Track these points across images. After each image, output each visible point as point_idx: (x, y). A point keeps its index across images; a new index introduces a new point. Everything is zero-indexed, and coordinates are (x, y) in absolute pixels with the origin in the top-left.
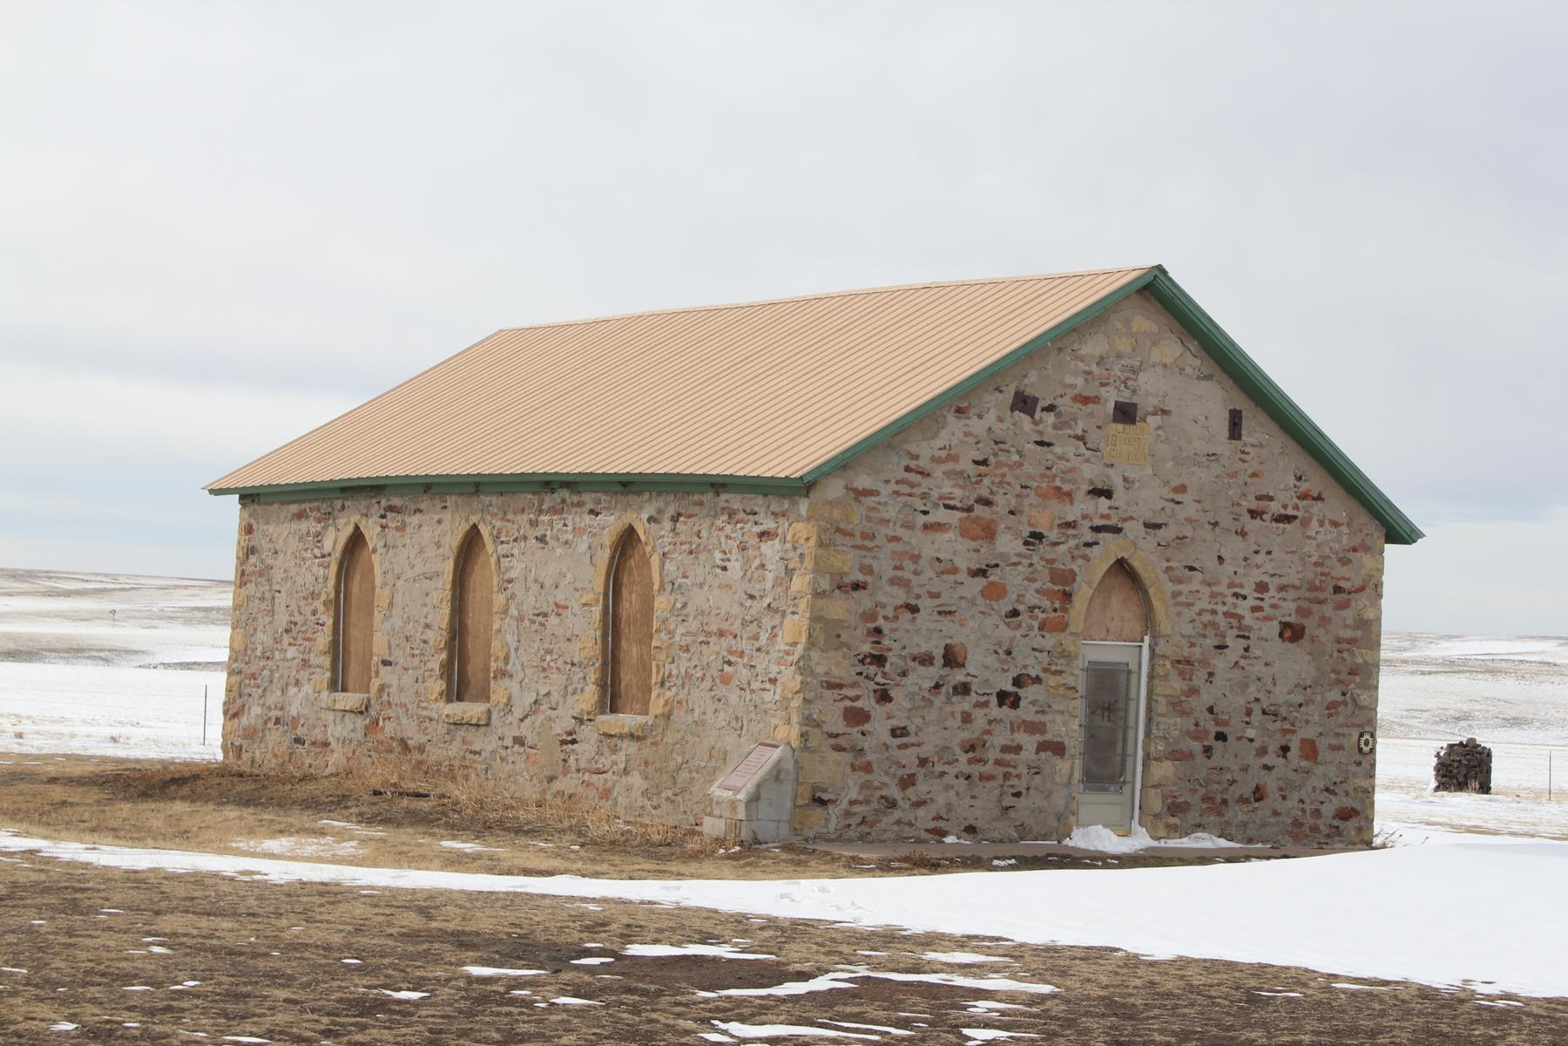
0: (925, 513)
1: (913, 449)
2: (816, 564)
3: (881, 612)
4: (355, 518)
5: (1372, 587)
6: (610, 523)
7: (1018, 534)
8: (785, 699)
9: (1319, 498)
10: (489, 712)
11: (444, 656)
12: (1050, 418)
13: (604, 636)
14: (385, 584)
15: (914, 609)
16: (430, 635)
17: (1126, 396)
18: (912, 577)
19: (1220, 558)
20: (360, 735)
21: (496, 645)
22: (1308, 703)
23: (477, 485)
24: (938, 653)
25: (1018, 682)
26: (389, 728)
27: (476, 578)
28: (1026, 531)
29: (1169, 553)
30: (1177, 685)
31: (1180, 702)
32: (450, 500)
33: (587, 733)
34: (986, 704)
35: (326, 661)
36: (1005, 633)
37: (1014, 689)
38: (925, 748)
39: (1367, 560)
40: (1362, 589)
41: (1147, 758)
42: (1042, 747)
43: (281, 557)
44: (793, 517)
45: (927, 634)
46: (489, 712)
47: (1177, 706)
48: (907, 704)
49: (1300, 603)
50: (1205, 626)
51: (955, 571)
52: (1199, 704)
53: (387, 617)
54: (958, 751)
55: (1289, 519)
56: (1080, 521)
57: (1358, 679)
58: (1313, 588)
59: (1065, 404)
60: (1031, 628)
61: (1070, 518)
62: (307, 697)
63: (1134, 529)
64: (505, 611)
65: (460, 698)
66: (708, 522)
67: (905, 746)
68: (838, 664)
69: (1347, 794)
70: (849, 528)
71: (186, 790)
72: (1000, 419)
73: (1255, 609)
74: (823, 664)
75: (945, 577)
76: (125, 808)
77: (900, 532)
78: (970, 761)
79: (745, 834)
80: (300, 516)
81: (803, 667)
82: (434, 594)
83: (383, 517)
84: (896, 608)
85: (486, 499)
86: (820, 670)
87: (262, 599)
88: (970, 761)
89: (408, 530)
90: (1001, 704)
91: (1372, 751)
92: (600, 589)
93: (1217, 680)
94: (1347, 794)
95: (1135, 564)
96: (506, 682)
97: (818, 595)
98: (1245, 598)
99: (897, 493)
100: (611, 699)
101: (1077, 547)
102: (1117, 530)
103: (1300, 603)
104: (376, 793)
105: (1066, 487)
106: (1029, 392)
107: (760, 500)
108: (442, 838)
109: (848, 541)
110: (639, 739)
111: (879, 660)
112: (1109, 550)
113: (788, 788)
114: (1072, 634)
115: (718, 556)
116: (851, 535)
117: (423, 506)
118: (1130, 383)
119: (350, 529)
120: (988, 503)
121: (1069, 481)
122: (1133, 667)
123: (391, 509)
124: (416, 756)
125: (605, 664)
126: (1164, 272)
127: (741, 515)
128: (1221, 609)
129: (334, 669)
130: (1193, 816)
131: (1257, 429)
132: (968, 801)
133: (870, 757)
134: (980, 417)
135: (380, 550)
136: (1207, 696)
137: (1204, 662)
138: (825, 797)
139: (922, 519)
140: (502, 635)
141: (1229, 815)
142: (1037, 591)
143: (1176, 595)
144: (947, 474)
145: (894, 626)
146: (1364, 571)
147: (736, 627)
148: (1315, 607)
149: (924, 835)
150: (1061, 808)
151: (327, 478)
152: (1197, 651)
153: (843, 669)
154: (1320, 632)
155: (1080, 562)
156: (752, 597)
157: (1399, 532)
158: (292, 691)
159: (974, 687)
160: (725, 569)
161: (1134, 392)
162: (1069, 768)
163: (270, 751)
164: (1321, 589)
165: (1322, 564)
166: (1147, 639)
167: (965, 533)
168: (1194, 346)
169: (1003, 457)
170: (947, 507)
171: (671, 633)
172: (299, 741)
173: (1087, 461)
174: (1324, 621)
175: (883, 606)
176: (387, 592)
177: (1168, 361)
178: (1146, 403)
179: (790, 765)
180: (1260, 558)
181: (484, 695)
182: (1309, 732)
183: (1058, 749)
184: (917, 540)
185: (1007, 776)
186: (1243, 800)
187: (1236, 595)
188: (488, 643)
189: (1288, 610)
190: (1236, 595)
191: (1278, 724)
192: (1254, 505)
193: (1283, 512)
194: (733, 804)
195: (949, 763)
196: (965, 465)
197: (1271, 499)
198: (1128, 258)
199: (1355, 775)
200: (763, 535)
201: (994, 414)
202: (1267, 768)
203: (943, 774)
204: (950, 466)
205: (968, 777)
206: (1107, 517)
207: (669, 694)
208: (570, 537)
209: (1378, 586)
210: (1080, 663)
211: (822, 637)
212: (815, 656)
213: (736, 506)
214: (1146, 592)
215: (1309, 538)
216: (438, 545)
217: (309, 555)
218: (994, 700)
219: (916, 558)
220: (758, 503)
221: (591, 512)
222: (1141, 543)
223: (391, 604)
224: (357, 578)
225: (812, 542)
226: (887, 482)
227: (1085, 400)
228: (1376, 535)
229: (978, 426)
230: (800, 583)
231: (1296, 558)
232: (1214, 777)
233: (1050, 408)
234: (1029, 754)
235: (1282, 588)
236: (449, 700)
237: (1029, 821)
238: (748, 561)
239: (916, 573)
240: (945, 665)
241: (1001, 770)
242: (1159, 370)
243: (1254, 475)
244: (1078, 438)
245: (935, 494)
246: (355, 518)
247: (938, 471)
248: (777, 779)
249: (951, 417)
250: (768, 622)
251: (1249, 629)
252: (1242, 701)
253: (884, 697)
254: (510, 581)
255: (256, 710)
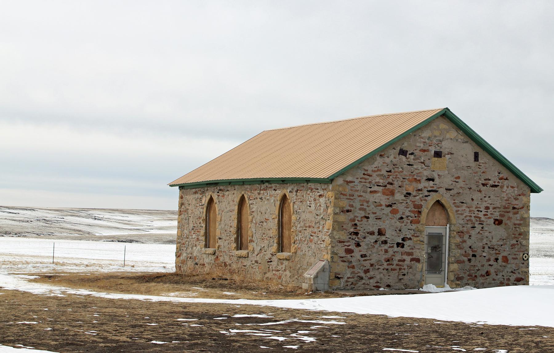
0: (370, 188)
1: (366, 168)
2: (334, 204)
3: (357, 219)
4: (211, 193)
5: (527, 207)
6: (279, 193)
7: (402, 193)
8: (326, 246)
9: (507, 179)
10: (248, 253)
11: (235, 236)
12: (412, 157)
13: (279, 228)
14: (219, 214)
15: (368, 218)
16: (232, 229)
17: (438, 149)
18: (367, 208)
19: (472, 199)
20: (213, 262)
21: (249, 232)
22: (505, 244)
23: (243, 182)
24: (376, 232)
25: (403, 239)
26: (221, 259)
27: (244, 212)
28: (405, 192)
29: (454, 198)
30: (458, 240)
31: (460, 245)
32: (236, 187)
33: (275, 259)
34: (393, 247)
35: (203, 238)
36: (398, 224)
37: (402, 242)
38: (372, 261)
39: (524, 199)
40: (523, 208)
41: (449, 263)
42: (412, 260)
43: (191, 206)
44: (328, 190)
45: (372, 225)
46: (248, 253)
47: (458, 246)
48: (366, 247)
49: (501, 213)
50: (468, 221)
51: (381, 205)
52: (466, 246)
53: (220, 224)
54: (383, 261)
55: (496, 186)
56: (423, 189)
57: (522, 237)
58: (505, 208)
59: (417, 153)
60: (407, 223)
61: (420, 188)
62: (198, 250)
63: (442, 191)
64: (252, 221)
65: (241, 249)
66: (305, 192)
67: (366, 260)
68: (343, 235)
69: (519, 273)
70: (345, 193)
71: (159, 280)
72: (395, 158)
73: (485, 215)
74: (338, 235)
75: (378, 207)
76: (136, 285)
77: (362, 194)
78: (388, 265)
79: (313, 288)
80: (196, 193)
81: (331, 236)
82: (232, 216)
83: (218, 192)
84: (361, 218)
85: (246, 186)
86: (337, 237)
87: (186, 219)
88: (388, 265)
89: (225, 196)
90: (398, 247)
91: (528, 259)
92: (277, 214)
93: (472, 238)
94: (519, 273)
95: (443, 202)
96: (252, 244)
97: (335, 214)
98: (481, 211)
99: (361, 182)
100: (281, 248)
101: (423, 197)
102: (436, 191)
103: (501, 213)
104: (214, 279)
105: (418, 178)
106: (404, 149)
107: (319, 185)
108: (225, 291)
109: (345, 197)
110: (288, 260)
111: (356, 234)
112: (434, 197)
113: (327, 274)
114: (422, 224)
115: (308, 202)
116: (346, 195)
117: (229, 189)
118: (439, 145)
119: (209, 196)
120: (391, 184)
121: (419, 176)
122: (444, 234)
123: (220, 190)
124: (228, 267)
125: (279, 237)
126: (449, 110)
127: (314, 190)
128: (473, 215)
129: (206, 241)
130: (465, 281)
131: (484, 158)
132: (387, 277)
133: (354, 264)
134: (388, 157)
135: (218, 203)
136: (469, 243)
137: (468, 232)
138: (339, 276)
139: (369, 190)
140: (251, 229)
141: (477, 280)
142: (409, 211)
143: (457, 211)
144: (378, 175)
145: (361, 223)
146: (523, 202)
147: (313, 225)
148: (506, 214)
149: (373, 288)
150: (419, 279)
151: (253, 177)
152: (465, 229)
153: (344, 236)
154: (508, 222)
155: (424, 202)
156: (317, 215)
157: (535, 189)
158: (194, 248)
159: (388, 242)
160: (310, 206)
161: (441, 148)
162: (423, 266)
163: (188, 267)
164: (508, 208)
165: (508, 200)
166: (448, 225)
167: (384, 193)
168: (461, 132)
169: (396, 170)
170: (378, 185)
171: (296, 227)
172: (197, 264)
173: (425, 170)
174: (509, 218)
175: (357, 217)
176: (220, 216)
177: (452, 138)
178: (444, 151)
179: (327, 267)
180: (486, 199)
181: (247, 248)
182: (505, 254)
183: (418, 260)
184: (368, 196)
185: (400, 269)
186: (482, 276)
187: (478, 211)
188: (248, 231)
189: (497, 215)
190: (478, 211)
191: (494, 252)
192: (484, 182)
193: (494, 184)
194: (310, 278)
195: (380, 265)
196: (384, 172)
197: (490, 180)
198: (438, 106)
199: (522, 267)
200: (320, 196)
201: (393, 156)
202: (490, 265)
203: (379, 269)
204: (379, 173)
205: (387, 270)
206: (433, 187)
207: (296, 246)
208: (269, 198)
209: (528, 207)
210: (425, 233)
211: (337, 227)
212: (335, 233)
213: (313, 187)
214: (447, 210)
215: (503, 192)
216: (233, 201)
217: (198, 205)
218: (395, 246)
219: (368, 202)
220: (318, 186)
221: (274, 190)
222: (445, 195)
223: (221, 220)
224: (212, 212)
225: (333, 198)
226: (357, 178)
227: (424, 151)
228: (527, 190)
229: (387, 160)
230: (330, 210)
231: (499, 198)
232: (472, 268)
233: (412, 154)
234: (408, 262)
235: (494, 208)
236: (237, 250)
237: (408, 283)
238: (316, 204)
239: (368, 206)
240: (378, 235)
241: (398, 267)
242: (449, 140)
243: (483, 172)
244: (422, 163)
245: (373, 182)
246: (211, 193)
247: (374, 174)
248: (323, 271)
249: (378, 158)
250: (322, 223)
251: (483, 221)
252: (481, 244)
253: (358, 245)
254: (253, 212)
255: (185, 255)
